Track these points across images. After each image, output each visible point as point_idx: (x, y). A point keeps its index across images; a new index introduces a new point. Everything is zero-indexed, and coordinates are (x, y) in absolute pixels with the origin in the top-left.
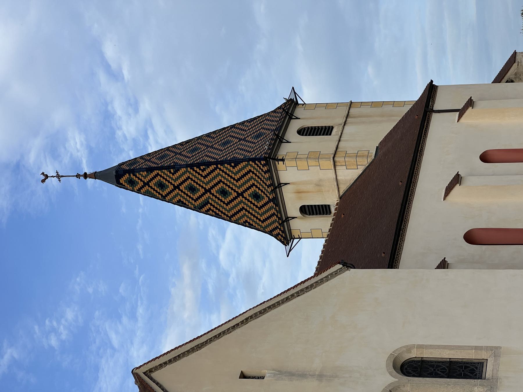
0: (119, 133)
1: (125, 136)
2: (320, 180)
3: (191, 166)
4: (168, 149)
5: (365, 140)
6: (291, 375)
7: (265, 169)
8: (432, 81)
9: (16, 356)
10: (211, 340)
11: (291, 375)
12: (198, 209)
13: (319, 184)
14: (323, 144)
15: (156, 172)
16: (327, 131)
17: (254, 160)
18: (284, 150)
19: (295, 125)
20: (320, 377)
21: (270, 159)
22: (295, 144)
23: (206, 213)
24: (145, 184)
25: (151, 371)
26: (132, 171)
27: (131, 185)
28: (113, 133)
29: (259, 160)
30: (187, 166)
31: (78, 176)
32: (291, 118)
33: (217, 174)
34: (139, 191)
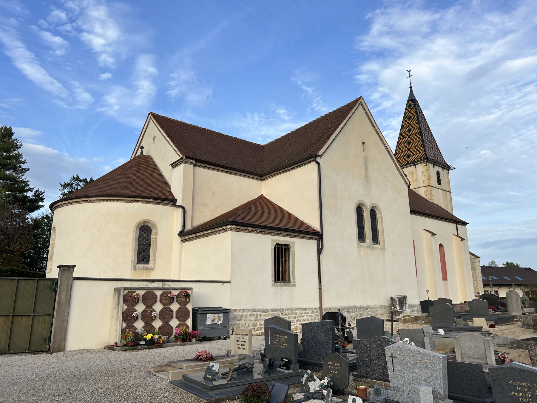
0: (392, 119)
1: (391, 122)
2: (418, 181)
3: (420, 129)
4: (425, 119)
5: (437, 198)
6: (366, 163)
7: (422, 158)
8: (75, 266)
9: (309, 92)
10: (376, 129)
11: (366, 163)
12: (401, 134)
13: (417, 180)
14: (434, 182)
15: (415, 115)
16: (439, 183)
17: (425, 153)
18: (430, 166)
19: (440, 170)
20: (366, 176)
21: (427, 160)
22: (433, 170)
23: (399, 137)
24: (410, 112)
25: (362, 104)
26: (415, 106)
27: (409, 106)
28: (392, 117)
29: (426, 156)
30: (420, 127)
31: (411, 84)
32: (443, 168)
33: (417, 140)
34: (406, 109)
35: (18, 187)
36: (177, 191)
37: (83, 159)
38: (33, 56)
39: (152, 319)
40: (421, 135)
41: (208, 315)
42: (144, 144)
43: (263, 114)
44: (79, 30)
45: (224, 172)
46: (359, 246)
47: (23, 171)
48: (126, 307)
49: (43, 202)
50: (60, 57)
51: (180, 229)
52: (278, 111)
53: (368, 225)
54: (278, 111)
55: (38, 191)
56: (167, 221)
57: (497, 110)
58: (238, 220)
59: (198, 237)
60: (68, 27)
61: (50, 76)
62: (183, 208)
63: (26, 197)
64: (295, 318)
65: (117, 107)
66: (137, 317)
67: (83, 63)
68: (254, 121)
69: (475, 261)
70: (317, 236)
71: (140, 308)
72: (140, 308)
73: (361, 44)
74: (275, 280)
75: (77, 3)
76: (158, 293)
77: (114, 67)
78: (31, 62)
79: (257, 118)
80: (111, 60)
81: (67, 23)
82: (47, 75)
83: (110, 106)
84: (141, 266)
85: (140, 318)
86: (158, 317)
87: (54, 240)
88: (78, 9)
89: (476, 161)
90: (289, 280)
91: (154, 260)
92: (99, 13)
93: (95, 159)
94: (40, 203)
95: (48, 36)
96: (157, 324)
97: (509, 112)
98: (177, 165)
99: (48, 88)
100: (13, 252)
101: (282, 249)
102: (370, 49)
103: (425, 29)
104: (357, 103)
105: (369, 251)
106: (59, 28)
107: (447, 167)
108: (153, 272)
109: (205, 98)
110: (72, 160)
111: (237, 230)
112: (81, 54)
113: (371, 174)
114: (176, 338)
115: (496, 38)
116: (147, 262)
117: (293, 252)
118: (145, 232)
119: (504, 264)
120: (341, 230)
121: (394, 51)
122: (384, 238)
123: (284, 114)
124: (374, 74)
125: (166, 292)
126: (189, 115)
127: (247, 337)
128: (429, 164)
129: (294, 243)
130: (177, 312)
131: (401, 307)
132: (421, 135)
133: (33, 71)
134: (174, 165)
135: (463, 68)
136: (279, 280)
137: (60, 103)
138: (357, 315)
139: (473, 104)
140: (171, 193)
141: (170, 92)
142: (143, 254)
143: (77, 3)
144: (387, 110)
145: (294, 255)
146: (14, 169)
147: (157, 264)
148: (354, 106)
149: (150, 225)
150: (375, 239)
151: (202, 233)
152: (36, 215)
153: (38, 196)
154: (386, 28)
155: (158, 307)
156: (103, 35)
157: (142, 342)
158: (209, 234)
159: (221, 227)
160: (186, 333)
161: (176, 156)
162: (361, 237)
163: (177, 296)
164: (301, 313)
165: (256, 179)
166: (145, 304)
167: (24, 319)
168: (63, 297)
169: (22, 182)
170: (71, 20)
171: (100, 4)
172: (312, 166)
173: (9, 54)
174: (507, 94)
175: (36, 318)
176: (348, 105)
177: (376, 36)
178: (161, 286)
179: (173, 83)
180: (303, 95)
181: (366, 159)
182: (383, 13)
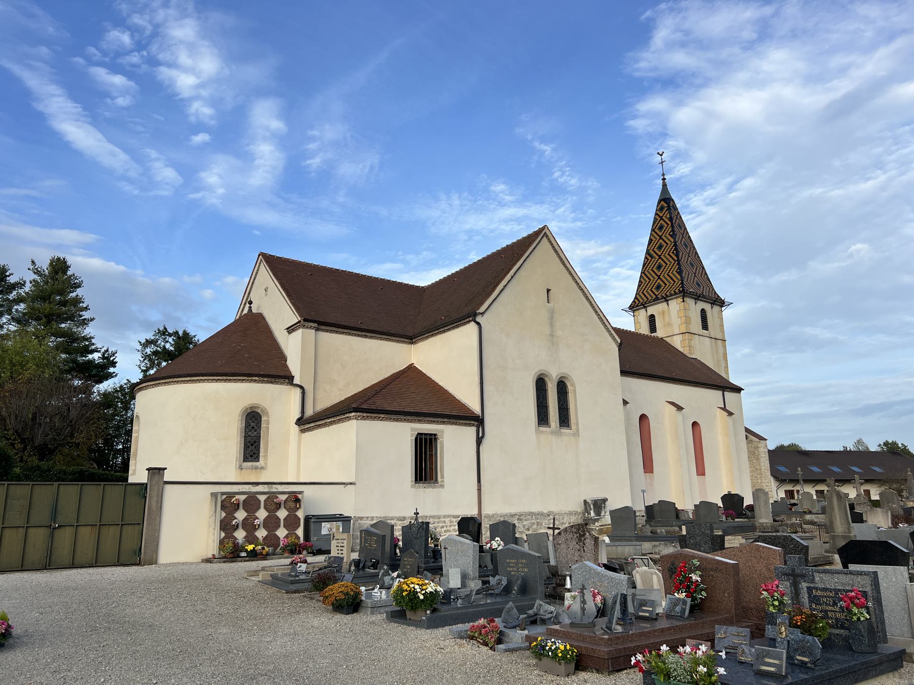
0: (692, 195)
3: (675, 245)
5: (701, 350)
6: (551, 318)
10: (568, 269)
11: (551, 318)
12: (648, 253)
13: (669, 324)
16: (705, 326)
17: (682, 283)
18: (690, 302)
19: (707, 307)
20: (552, 335)
21: (684, 293)
22: (694, 308)
23: (646, 258)
24: (661, 218)
26: (669, 208)
27: (660, 209)
29: (682, 287)
30: (675, 242)
31: (663, 175)
34: (656, 214)
35: (77, 345)
36: (294, 365)
37: (166, 280)
38: (80, 109)
39: (255, 528)
40: (677, 256)
41: (323, 524)
42: (252, 297)
43: (466, 194)
44: (154, 62)
45: (359, 336)
46: (538, 432)
47: (85, 322)
48: (224, 514)
49: (115, 367)
50: (124, 108)
51: (298, 415)
52: (493, 188)
53: (553, 403)
54: (493, 188)
55: (107, 350)
56: (281, 405)
57: (879, 172)
58: (365, 406)
59: (319, 426)
60: (135, 59)
61: (110, 140)
62: (301, 387)
63: (91, 362)
64: (443, 527)
65: (221, 191)
66: (237, 526)
67: (163, 119)
68: (451, 205)
69: (759, 445)
70: (477, 421)
71: (241, 515)
72: (241, 515)
73: (636, 66)
74: (416, 480)
75: (147, 17)
76: (262, 498)
77: (213, 122)
78: (78, 120)
79: (456, 202)
80: (207, 111)
81: (131, 51)
82: (105, 140)
83: (209, 188)
84: (249, 464)
85: (240, 527)
86: (262, 526)
87: (138, 432)
88: (149, 28)
89: (845, 264)
90: (436, 480)
91: (266, 457)
92: (184, 31)
93: (187, 279)
94: (111, 370)
95: (101, 74)
96: (261, 533)
97: (903, 174)
98: (294, 330)
99: (106, 161)
100: (78, 445)
101: (426, 439)
102: (651, 74)
103: (748, 34)
104: (541, 234)
105: (554, 439)
106: (120, 61)
107: (719, 302)
108: (264, 472)
109: (367, 170)
110: (148, 281)
111: (363, 418)
112: (156, 95)
113: (559, 333)
114: (284, 550)
115: (873, 47)
116: (257, 459)
117: (442, 443)
118: (253, 421)
119: (880, 445)
120: (511, 410)
121: (694, 75)
122: (577, 421)
123: (502, 192)
124: (660, 118)
125: (272, 496)
126: (341, 199)
127: (345, 542)
128: (687, 300)
129: (442, 431)
130: (285, 520)
131: (598, 513)
132: (677, 256)
133: (80, 134)
134: (291, 330)
135: (815, 100)
136: (421, 480)
137: (127, 188)
138: (533, 524)
139: (837, 163)
140: (287, 367)
141: (308, 162)
142: (252, 449)
143: (147, 17)
144: (683, 180)
145: (442, 447)
146: (71, 318)
147: (269, 461)
148: (529, 246)
149: (259, 411)
150: (564, 420)
151: (323, 422)
152: (106, 386)
153: (107, 358)
154: (679, 36)
155: (262, 514)
156: (195, 66)
157: (243, 554)
158: (331, 423)
159: (344, 414)
160: (295, 545)
161: (293, 318)
162: (543, 418)
163: (285, 501)
164: (451, 522)
165: (403, 342)
166: (246, 511)
167: (112, 529)
168: (154, 504)
169: (85, 339)
170: (140, 46)
171: (186, 17)
172: (471, 328)
173: (40, 107)
174: (897, 144)
175: (125, 528)
176: (529, 236)
177: (662, 51)
178: (266, 490)
179: (312, 146)
180: (535, 158)
181: (552, 313)
182: (671, 10)
